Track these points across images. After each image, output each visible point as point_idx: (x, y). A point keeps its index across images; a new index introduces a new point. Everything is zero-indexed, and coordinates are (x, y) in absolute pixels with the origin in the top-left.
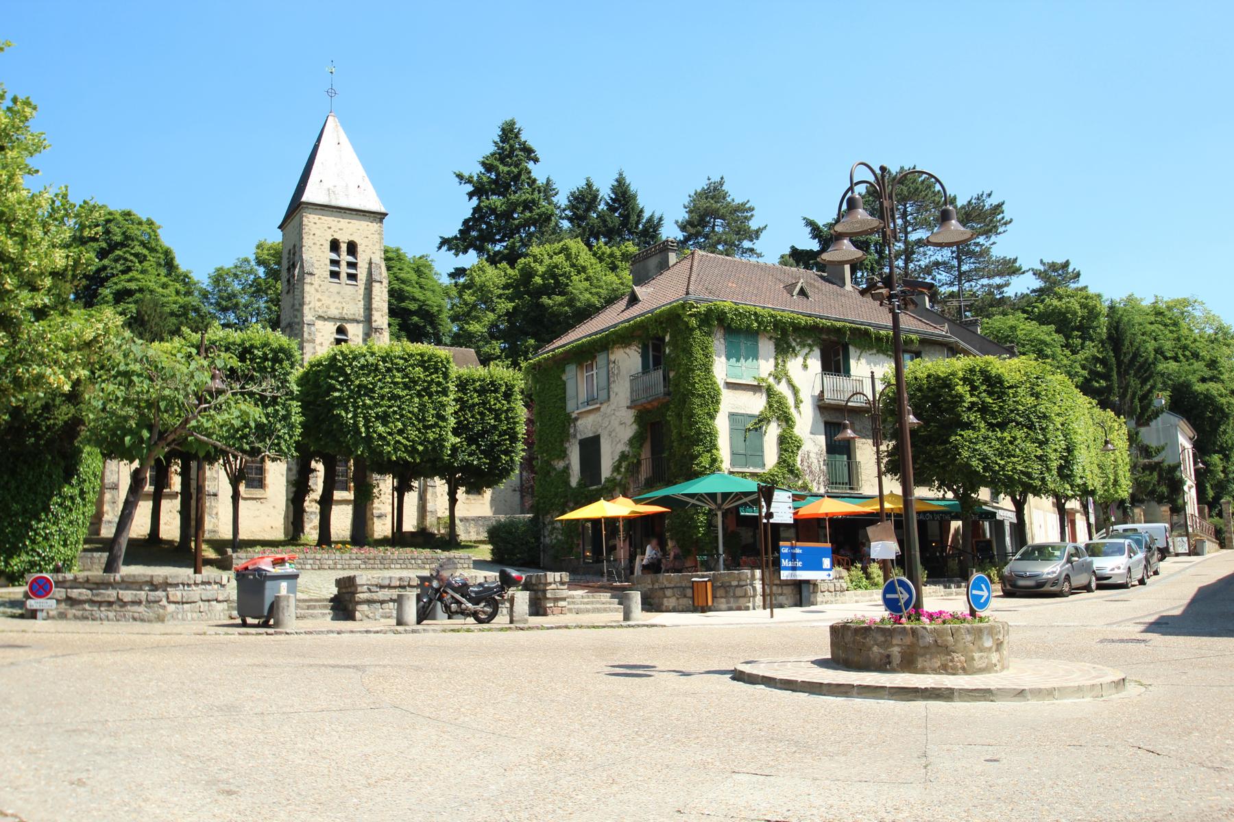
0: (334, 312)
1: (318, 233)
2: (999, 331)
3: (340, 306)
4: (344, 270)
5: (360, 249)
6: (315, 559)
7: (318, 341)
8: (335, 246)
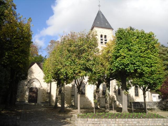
4: (104, 41)
5: (107, 37)
8: (101, 36)
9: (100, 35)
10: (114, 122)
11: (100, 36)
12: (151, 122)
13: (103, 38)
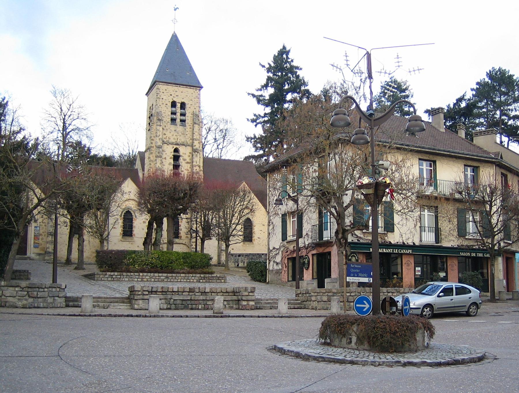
0: (172, 140)
1: (164, 98)
2: (72, 191)
3: (176, 138)
4: (178, 117)
5: (187, 106)
6: (172, 276)
7: (164, 156)
8: (174, 104)
9: (171, 101)
10: (137, 277)
11: (170, 105)
12: (183, 278)
13: (179, 110)
